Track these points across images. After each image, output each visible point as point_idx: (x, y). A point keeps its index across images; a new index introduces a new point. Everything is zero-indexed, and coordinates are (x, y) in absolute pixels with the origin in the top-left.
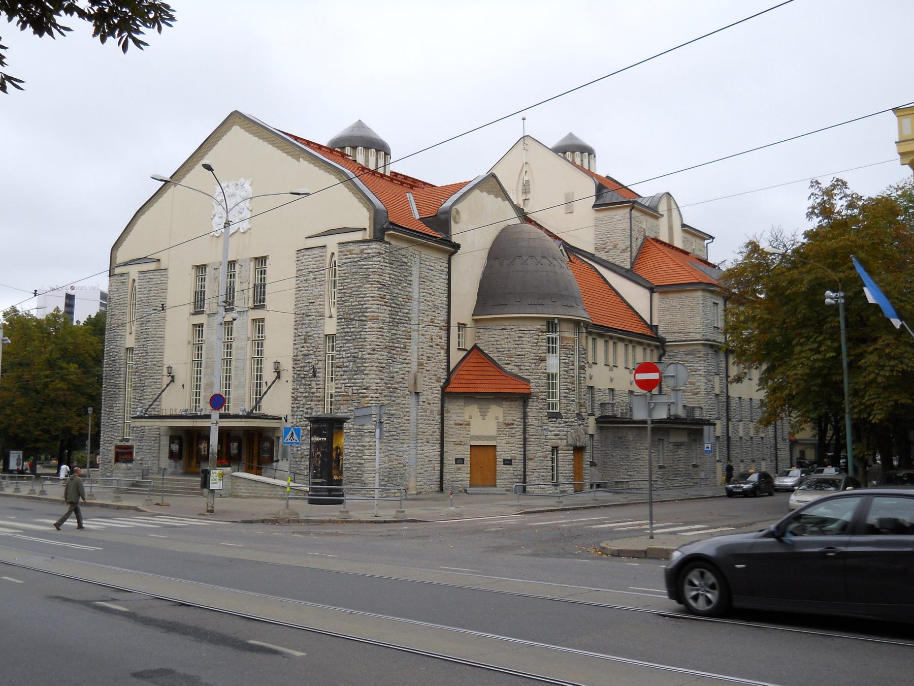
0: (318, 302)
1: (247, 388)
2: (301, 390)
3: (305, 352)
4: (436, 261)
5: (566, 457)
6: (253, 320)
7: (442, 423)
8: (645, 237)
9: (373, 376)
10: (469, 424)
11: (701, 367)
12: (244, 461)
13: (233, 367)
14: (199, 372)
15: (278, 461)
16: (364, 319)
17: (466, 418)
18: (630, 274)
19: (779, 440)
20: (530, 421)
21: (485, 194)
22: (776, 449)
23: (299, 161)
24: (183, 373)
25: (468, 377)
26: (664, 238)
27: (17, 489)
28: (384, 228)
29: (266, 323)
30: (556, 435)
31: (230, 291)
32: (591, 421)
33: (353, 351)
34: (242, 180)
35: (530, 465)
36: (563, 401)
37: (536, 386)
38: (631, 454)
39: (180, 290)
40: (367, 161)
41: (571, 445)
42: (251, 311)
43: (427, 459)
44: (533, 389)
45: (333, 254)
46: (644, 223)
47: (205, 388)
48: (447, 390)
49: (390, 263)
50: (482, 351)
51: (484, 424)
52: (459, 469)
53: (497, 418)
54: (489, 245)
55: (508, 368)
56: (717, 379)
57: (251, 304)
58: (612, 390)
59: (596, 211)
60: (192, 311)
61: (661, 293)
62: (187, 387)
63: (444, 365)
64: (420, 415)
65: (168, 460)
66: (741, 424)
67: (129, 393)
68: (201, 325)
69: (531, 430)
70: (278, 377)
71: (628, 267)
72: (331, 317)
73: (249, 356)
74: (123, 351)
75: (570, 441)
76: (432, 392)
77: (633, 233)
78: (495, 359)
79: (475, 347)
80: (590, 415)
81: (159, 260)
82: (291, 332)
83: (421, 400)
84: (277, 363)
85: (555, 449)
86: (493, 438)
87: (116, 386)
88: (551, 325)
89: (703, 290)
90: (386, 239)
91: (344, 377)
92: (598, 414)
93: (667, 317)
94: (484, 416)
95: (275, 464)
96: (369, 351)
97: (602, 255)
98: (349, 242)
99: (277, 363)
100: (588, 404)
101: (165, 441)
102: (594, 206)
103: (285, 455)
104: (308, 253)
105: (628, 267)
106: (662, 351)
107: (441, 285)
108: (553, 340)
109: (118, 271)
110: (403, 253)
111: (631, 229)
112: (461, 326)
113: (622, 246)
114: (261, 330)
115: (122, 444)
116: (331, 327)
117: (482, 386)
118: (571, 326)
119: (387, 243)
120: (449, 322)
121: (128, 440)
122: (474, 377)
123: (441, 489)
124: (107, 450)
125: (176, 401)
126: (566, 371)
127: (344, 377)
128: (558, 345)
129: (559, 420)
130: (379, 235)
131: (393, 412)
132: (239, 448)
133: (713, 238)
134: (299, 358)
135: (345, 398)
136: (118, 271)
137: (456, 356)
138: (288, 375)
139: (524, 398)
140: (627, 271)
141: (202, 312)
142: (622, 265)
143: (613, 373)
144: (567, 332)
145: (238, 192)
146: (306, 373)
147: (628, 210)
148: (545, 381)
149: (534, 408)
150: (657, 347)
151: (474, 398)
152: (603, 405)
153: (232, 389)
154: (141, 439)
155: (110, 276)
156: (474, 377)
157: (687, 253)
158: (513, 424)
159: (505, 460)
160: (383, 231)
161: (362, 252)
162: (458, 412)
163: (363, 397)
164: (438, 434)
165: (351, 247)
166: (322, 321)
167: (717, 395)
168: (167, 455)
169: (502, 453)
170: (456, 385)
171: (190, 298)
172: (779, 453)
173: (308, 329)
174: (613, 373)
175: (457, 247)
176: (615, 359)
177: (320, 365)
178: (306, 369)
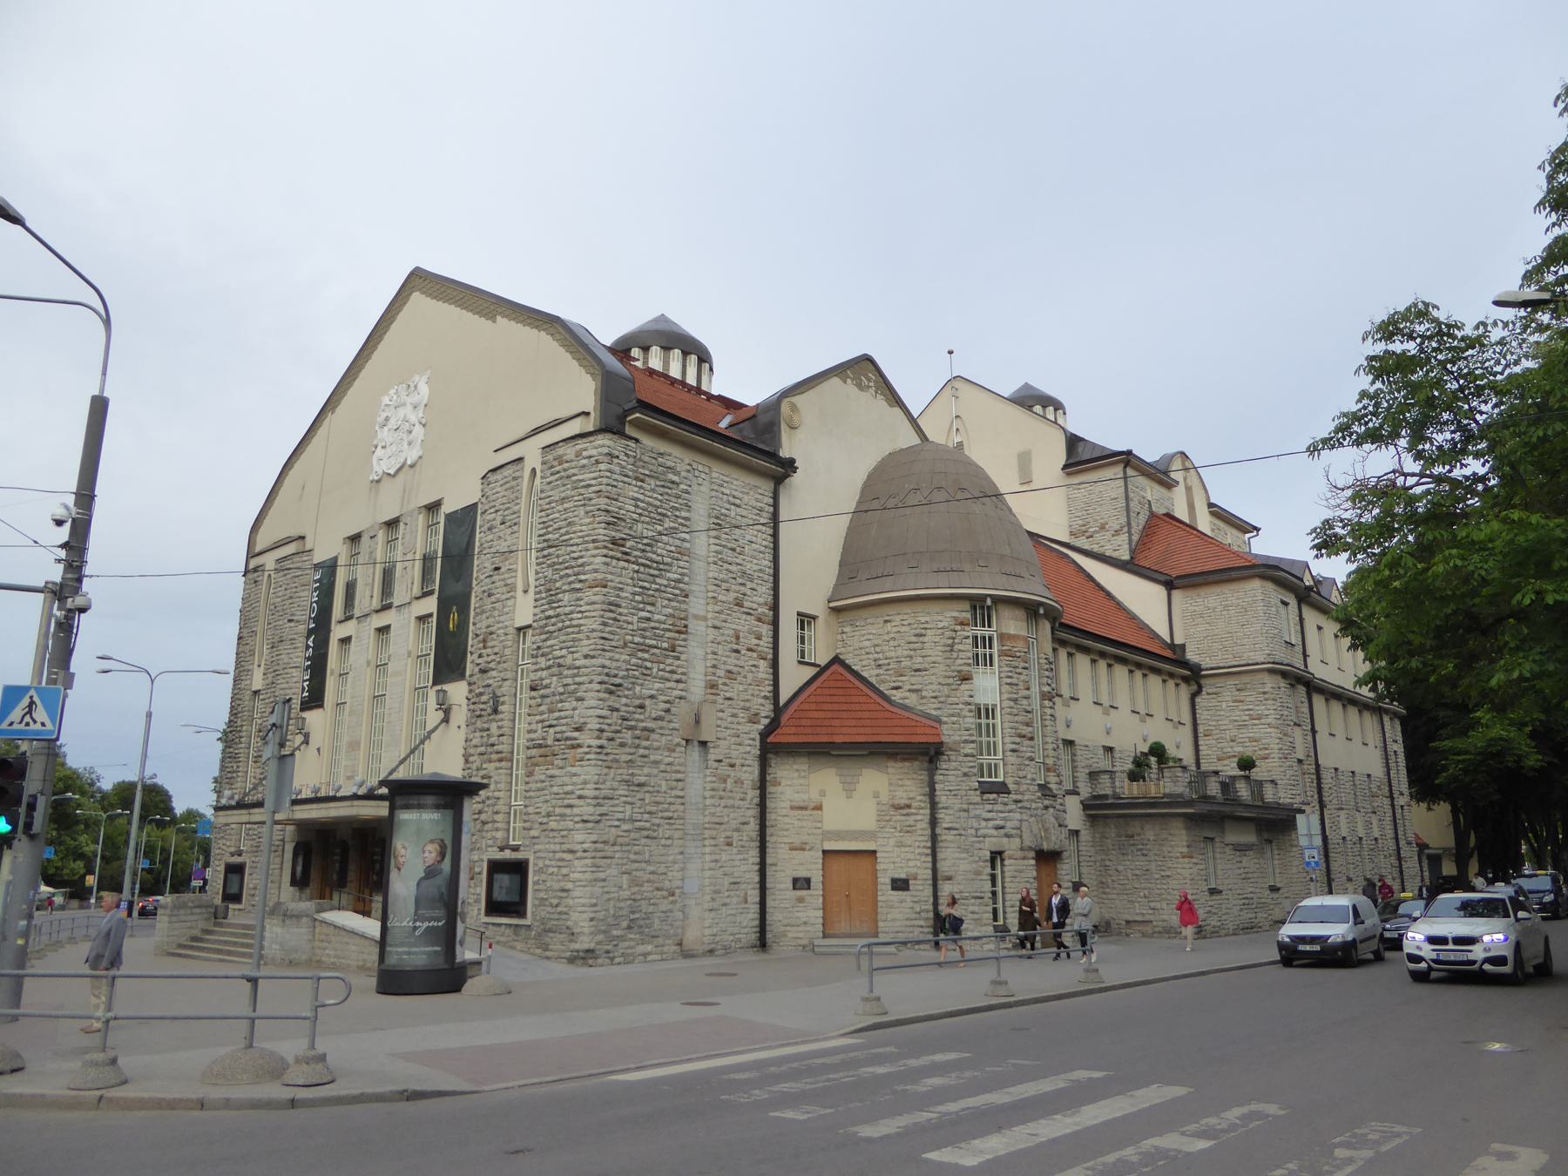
4: (749, 491)
7: (763, 806)
8: (1153, 515)
9: (593, 703)
10: (819, 808)
11: (1270, 711)
12: (352, 886)
16: (578, 586)
17: (814, 796)
19: (1402, 843)
20: (942, 799)
22: (1399, 859)
25: (816, 715)
30: (998, 828)
32: (1073, 806)
33: (558, 653)
34: (417, 378)
36: (1012, 758)
38: (1153, 866)
40: (666, 363)
41: (1030, 848)
43: (727, 880)
44: (949, 735)
46: (1151, 491)
49: (636, 479)
50: (848, 668)
51: (846, 805)
53: (876, 795)
54: (860, 478)
55: (897, 696)
56: (1298, 732)
58: (1109, 750)
59: (1069, 474)
63: (767, 689)
64: (709, 790)
66: (1342, 813)
69: (946, 819)
71: (1126, 557)
76: (739, 743)
77: (1132, 504)
78: (873, 680)
79: (836, 660)
80: (1069, 793)
83: (712, 757)
85: (996, 856)
86: (871, 835)
91: (543, 708)
92: (1085, 790)
93: (1201, 628)
94: (849, 791)
96: (585, 651)
97: (1082, 543)
100: (1066, 772)
102: (1065, 467)
104: (498, 476)
106: (1195, 687)
108: (987, 642)
110: (669, 464)
111: (1127, 498)
112: (805, 620)
117: (845, 730)
118: (1021, 614)
119: (631, 438)
120: (775, 608)
121: (515, 849)
122: (829, 715)
123: (762, 944)
126: (1015, 700)
129: (1003, 798)
130: (612, 425)
131: (643, 779)
133: (1258, 529)
137: (793, 678)
139: (929, 754)
140: (1127, 562)
142: (1115, 555)
143: (1115, 716)
144: (1011, 623)
147: (1119, 468)
148: (970, 721)
149: (953, 779)
150: (1186, 679)
151: (828, 754)
152: (1093, 775)
156: (829, 715)
158: (909, 806)
159: (795, 881)
160: (622, 418)
161: (578, 454)
162: (796, 782)
163: (573, 747)
164: (753, 826)
166: (509, 603)
167: (1300, 761)
169: (889, 867)
172: (1405, 865)
174: (1115, 716)
175: (789, 466)
176: (1112, 694)
177: (506, 688)
178: (484, 698)
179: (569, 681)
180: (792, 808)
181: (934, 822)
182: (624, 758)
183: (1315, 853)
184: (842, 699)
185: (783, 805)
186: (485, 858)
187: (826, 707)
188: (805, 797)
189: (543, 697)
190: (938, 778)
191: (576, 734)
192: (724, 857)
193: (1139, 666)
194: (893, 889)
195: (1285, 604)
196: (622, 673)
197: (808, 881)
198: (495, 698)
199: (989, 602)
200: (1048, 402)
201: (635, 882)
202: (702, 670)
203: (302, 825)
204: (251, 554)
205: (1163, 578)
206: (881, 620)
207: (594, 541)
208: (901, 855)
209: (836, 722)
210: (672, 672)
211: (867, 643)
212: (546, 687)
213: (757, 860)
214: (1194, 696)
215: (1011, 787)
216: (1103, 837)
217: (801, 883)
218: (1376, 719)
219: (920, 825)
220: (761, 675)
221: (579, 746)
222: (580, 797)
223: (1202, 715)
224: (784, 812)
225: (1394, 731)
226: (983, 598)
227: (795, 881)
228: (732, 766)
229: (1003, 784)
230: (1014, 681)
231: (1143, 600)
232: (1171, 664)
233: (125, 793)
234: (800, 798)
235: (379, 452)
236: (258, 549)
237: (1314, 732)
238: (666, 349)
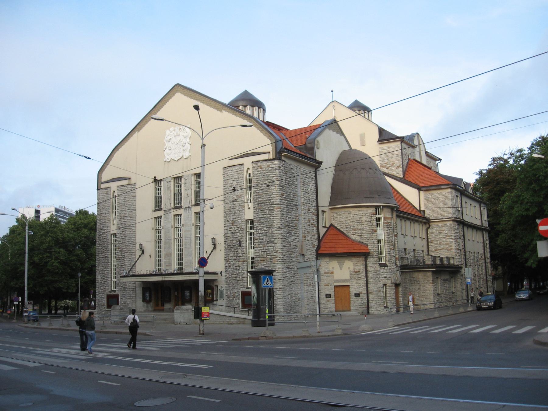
0: (239, 200)
1: (193, 256)
2: (231, 255)
3: (234, 231)
5: (390, 290)
6: (195, 213)
8: (409, 159)
9: (280, 244)
10: (332, 273)
13: (183, 243)
14: (160, 247)
15: (217, 300)
17: (331, 269)
18: (404, 180)
20: (369, 269)
23: (221, 111)
24: (150, 248)
25: (330, 244)
26: (418, 159)
27: (51, 324)
28: (281, 152)
29: (183, 217)
31: (178, 194)
33: (266, 229)
35: (371, 296)
37: (372, 248)
39: (145, 198)
43: (310, 296)
45: (114, 192)
47: (165, 257)
48: (319, 252)
50: (336, 228)
52: (328, 301)
53: (349, 268)
55: (353, 237)
57: (173, 206)
58: (405, 249)
60: (153, 209)
61: (425, 191)
62: (153, 256)
65: (142, 303)
67: (114, 261)
68: (160, 217)
69: (370, 275)
70: (215, 248)
71: (401, 176)
72: (249, 208)
73: (193, 235)
74: (109, 236)
75: (393, 281)
78: (345, 232)
79: (331, 225)
81: (130, 178)
82: (222, 219)
83: (306, 259)
84: (213, 239)
87: (106, 258)
88: (378, 209)
89: (451, 188)
90: (283, 158)
91: (260, 246)
94: (341, 267)
95: (215, 302)
96: (276, 229)
98: (259, 161)
99: (213, 239)
101: (139, 291)
102: (379, 141)
103: (221, 297)
106: (428, 226)
107: (312, 187)
109: (103, 186)
113: (397, 164)
114: (180, 221)
115: (111, 293)
116: (249, 214)
118: (389, 210)
121: (115, 291)
122: (334, 244)
124: (102, 298)
125: (146, 266)
127: (260, 246)
130: (278, 157)
132: (178, 293)
133: (441, 160)
134: (228, 235)
135: (262, 259)
136: (103, 186)
137: (322, 231)
138: (221, 246)
139: (366, 255)
141: (161, 210)
142: (397, 175)
143: (412, 238)
145: (181, 133)
146: (233, 245)
147: (399, 143)
149: (371, 262)
150: (425, 223)
153: (183, 257)
154: (124, 290)
155: (98, 190)
157: (430, 168)
158: (359, 272)
159: (326, 295)
165: (261, 164)
168: (141, 300)
169: (353, 290)
170: (324, 249)
171: (151, 205)
173: (234, 217)
177: (244, 239)
179: (270, 238)
180: (325, 273)
181: (367, 276)
182: (288, 260)
184: (336, 238)
186: (240, 291)
187: (332, 241)
189: (260, 242)
190: (368, 263)
192: (309, 289)
193: (404, 218)
195: (457, 196)
197: (330, 295)
198: (239, 241)
200: (366, 110)
201: (291, 297)
203: (144, 283)
204: (99, 182)
206: (347, 213)
208: (357, 286)
209: (336, 246)
212: (262, 239)
214: (427, 229)
215: (388, 265)
216: (405, 278)
217: (328, 296)
218: (481, 232)
219: (363, 277)
225: (486, 237)
227: (326, 295)
229: (385, 264)
231: (410, 194)
232: (420, 219)
235: (167, 150)
236: (103, 180)
238: (253, 106)
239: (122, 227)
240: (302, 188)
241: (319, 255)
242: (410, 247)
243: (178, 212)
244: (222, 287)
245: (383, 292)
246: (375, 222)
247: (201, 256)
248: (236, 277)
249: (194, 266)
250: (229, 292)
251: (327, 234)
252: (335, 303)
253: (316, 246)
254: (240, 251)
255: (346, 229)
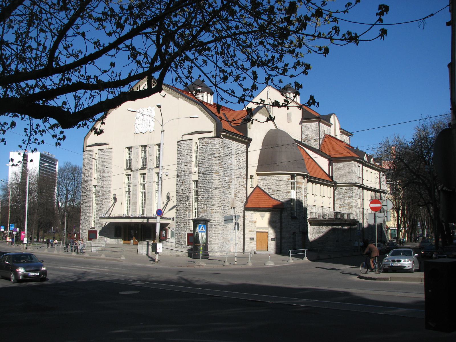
0: (189, 165)
15: (169, 239)
17: (254, 219)
18: (318, 152)
21: (261, 115)
23: (357, 148)
29: (147, 176)
35: (283, 240)
42: (154, 169)
47: (132, 205)
48: (246, 206)
55: (273, 196)
79: (257, 186)
83: (235, 211)
85: (294, 233)
88: (293, 176)
95: (168, 240)
98: (204, 138)
99: (168, 193)
105: (318, 148)
108: (293, 184)
115: (92, 230)
119: (222, 138)
121: (94, 228)
128: (296, 186)
132: (138, 232)
135: (203, 210)
137: (250, 191)
150: (333, 186)
165: (206, 140)
167: (359, 208)
170: (250, 204)
175: (251, 140)
180: (250, 222)
182: (222, 212)
183: (360, 232)
185: (248, 221)
188: (252, 219)
191: (213, 207)
194: (272, 240)
195: (359, 166)
196: (221, 193)
197: (253, 238)
198: (187, 196)
199: (295, 175)
201: (223, 239)
202: (234, 191)
205: (329, 157)
207: (216, 163)
210: (229, 192)
211: (266, 183)
213: (243, 234)
217: (252, 239)
220: (244, 191)
221: (213, 209)
222: (214, 221)
223: (336, 196)
224: (248, 223)
226: (294, 174)
228: (239, 213)
230: (299, 193)
233: (371, 227)
234: (251, 220)
237: (363, 200)
239: (101, 178)
240: (236, 159)
241: (247, 209)
242: (319, 204)
243: (143, 171)
244: (173, 229)
245: (293, 238)
246: (290, 185)
247: (159, 208)
248: (184, 222)
249: (154, 213)
250: (178, 233)
251: (253, 193)
252: (257, 244)
253: (244, 202)
254: (187, 203)
255: (267, 190)
